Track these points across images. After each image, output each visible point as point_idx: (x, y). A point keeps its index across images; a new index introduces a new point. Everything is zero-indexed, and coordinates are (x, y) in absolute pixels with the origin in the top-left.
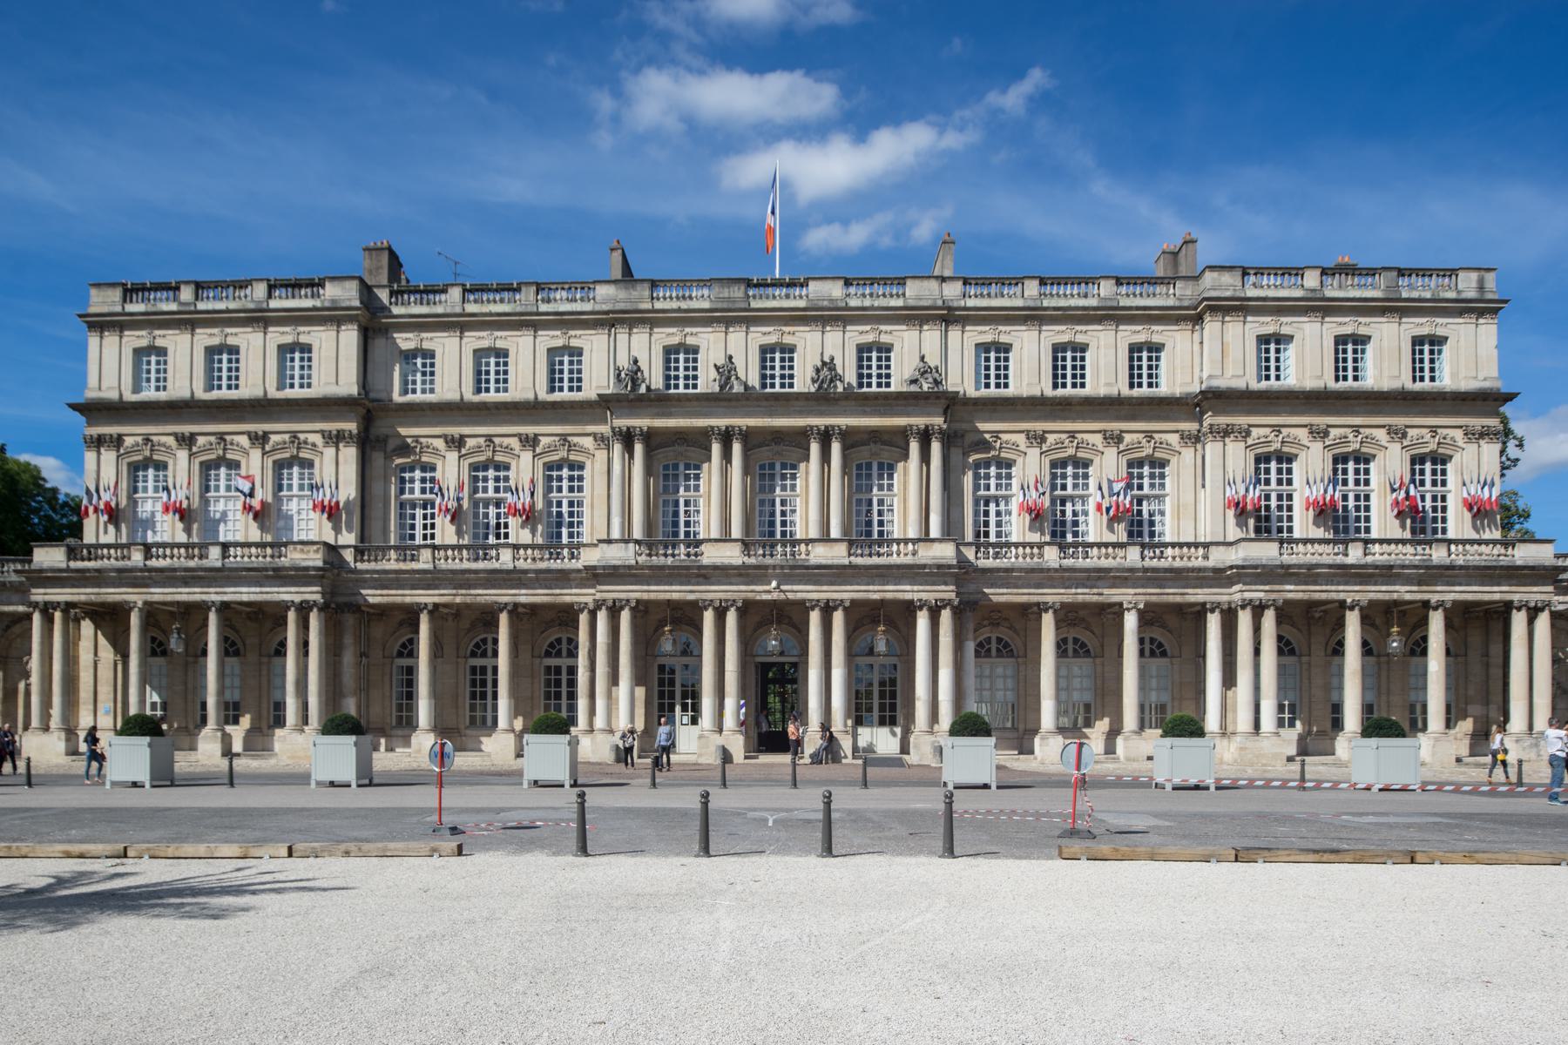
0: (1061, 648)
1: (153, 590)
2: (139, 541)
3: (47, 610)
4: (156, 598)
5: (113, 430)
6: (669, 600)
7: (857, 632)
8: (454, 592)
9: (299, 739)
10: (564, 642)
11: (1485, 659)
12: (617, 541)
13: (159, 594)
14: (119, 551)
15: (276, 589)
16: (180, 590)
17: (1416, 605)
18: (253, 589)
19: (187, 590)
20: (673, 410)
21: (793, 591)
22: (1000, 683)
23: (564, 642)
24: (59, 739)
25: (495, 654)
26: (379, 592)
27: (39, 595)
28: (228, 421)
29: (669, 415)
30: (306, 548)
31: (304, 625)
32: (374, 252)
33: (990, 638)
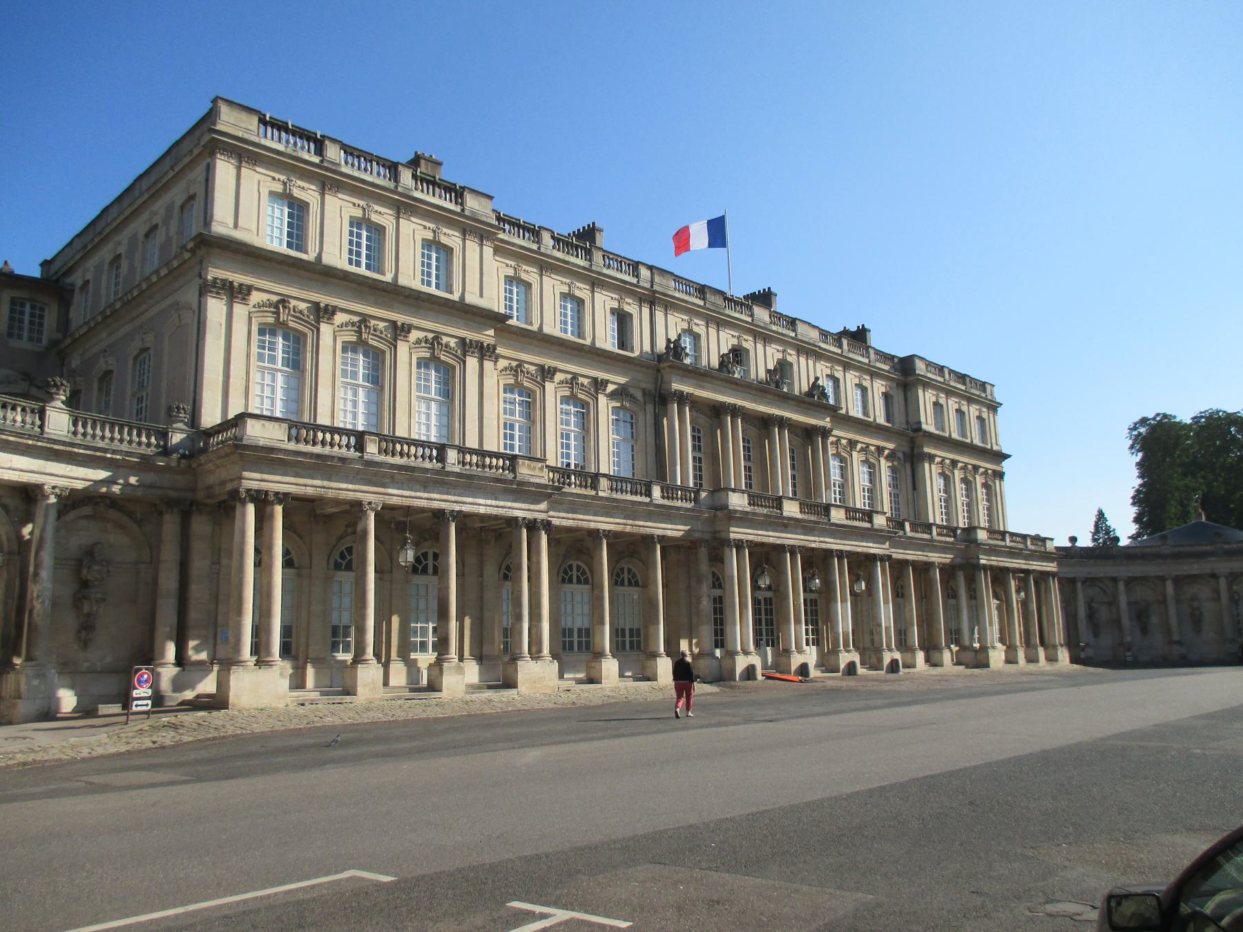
0: (616, 580)
1: (390, 491)
2: (457, 443)
3: (262, 501)
4: (395, 501)
5: (238, 278)
6: (409, 507)
7: (113, 514)
8: (624, 521)
9: (264, 674)
10: (430, 556)
11: (480, 579)
12: (277, 420)
13: (398, 496)
14: (501, 460)
15: (509, 504)
16: (419, 494)
17: (425, 515)
18: (489, 502)
19: (425, 495)
20: (705, 384)
21: (558, 517)
22: (578, 610)
23: (430, 556)
24: (281, 675)
25: (805, 600)
26: (570, 516)
27: (253, 480)
28: (376, 304)
29: (702, 388)
30: (534, 464)
31: (263, 520)
32: (429, 163)
33: (572, 565)
